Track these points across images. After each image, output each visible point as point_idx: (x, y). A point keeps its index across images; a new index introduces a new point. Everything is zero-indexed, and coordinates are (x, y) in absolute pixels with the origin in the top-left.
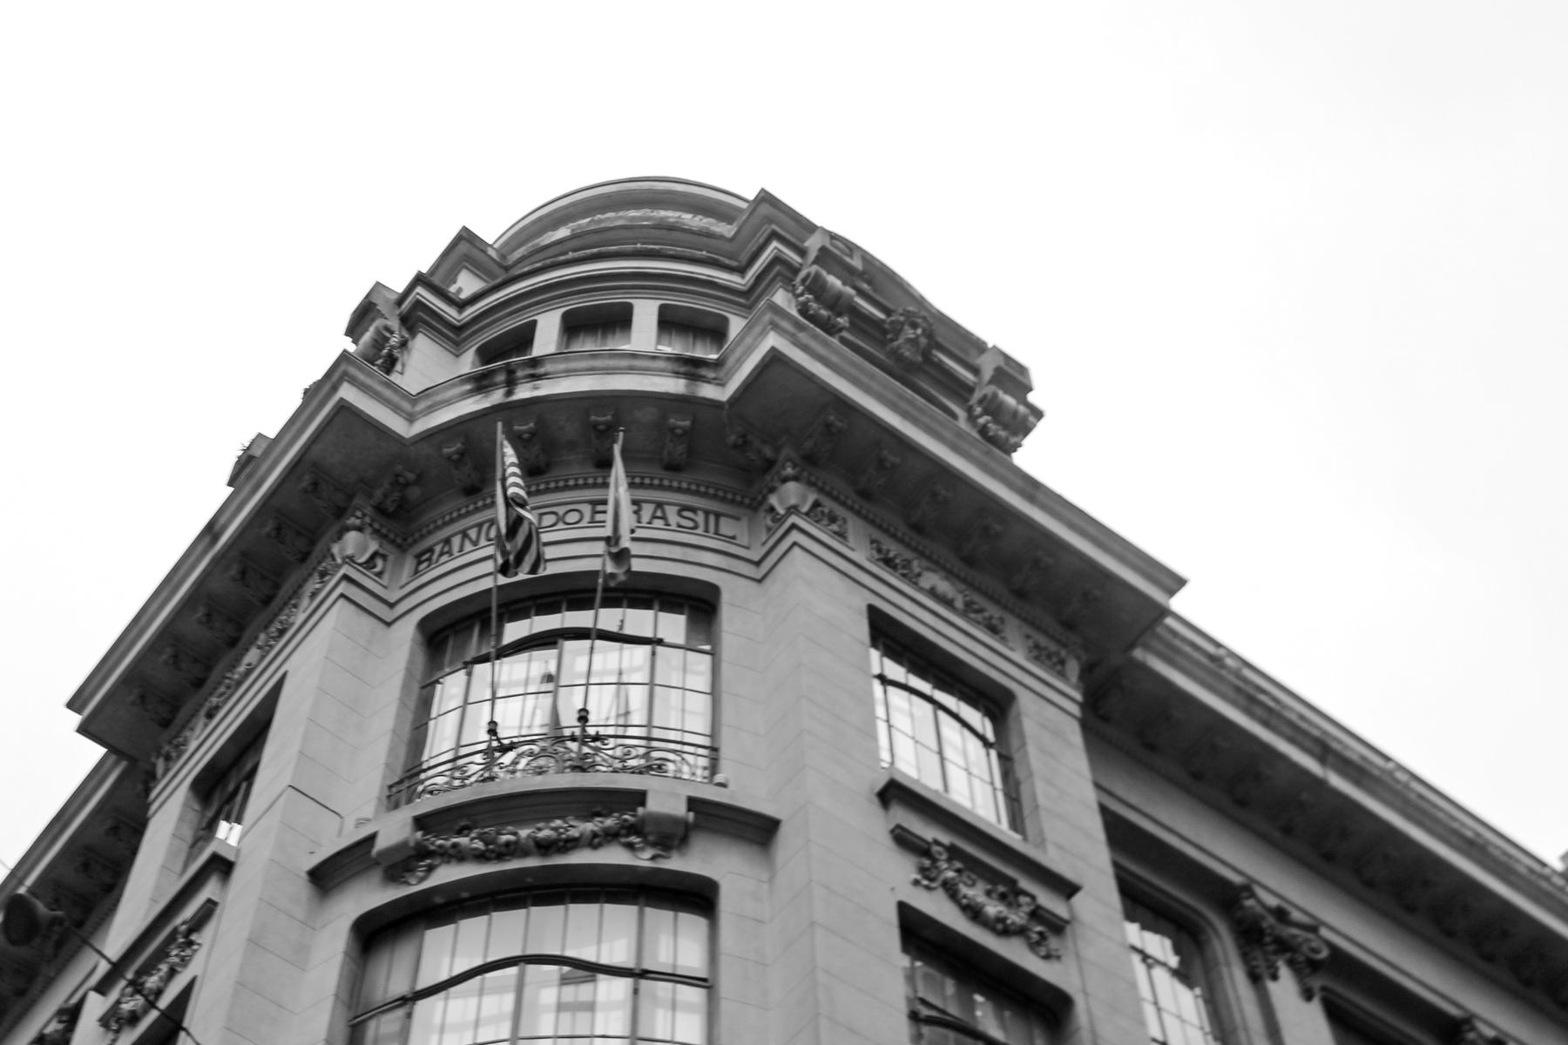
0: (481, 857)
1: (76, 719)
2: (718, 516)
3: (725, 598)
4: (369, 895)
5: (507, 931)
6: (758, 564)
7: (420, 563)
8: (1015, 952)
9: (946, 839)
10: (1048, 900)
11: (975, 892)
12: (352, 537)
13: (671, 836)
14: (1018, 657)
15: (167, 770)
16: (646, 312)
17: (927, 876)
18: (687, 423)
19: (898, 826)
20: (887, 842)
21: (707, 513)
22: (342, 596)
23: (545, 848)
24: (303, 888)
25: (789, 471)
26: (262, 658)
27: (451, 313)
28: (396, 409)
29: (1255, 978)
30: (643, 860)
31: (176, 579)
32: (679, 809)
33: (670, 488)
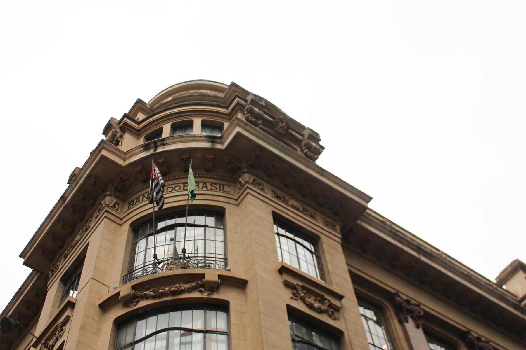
0: (153, 297)
1: (22, 260)
2: (223, 185)
3: (227, 211)
4: (118, 312)
5: (162, 320)
6: (237, 200)
7: (129, 205)
8: (324, 318)
9: (300, 284)
10: (334, 301)
11: (311, 300)
12: (108, 198)
13: (213, 287)
14: (320, 225)
15: (52, 275)
16: (197, 123)
17: (295, 296)
18: (212, 157)
19: (285, 280)
20: (282, 285)
21: (220, 185)
22: (105, 217)
23: (173, 293)
24: (97, 310)
25: (245, 170)
26: (81, 238)
27: (136, 126)
28: (120, 157)
29: (401, 322)
30: (205, 295)
31: (52, 214)
32: (216, 279)
33: (208, 178)
